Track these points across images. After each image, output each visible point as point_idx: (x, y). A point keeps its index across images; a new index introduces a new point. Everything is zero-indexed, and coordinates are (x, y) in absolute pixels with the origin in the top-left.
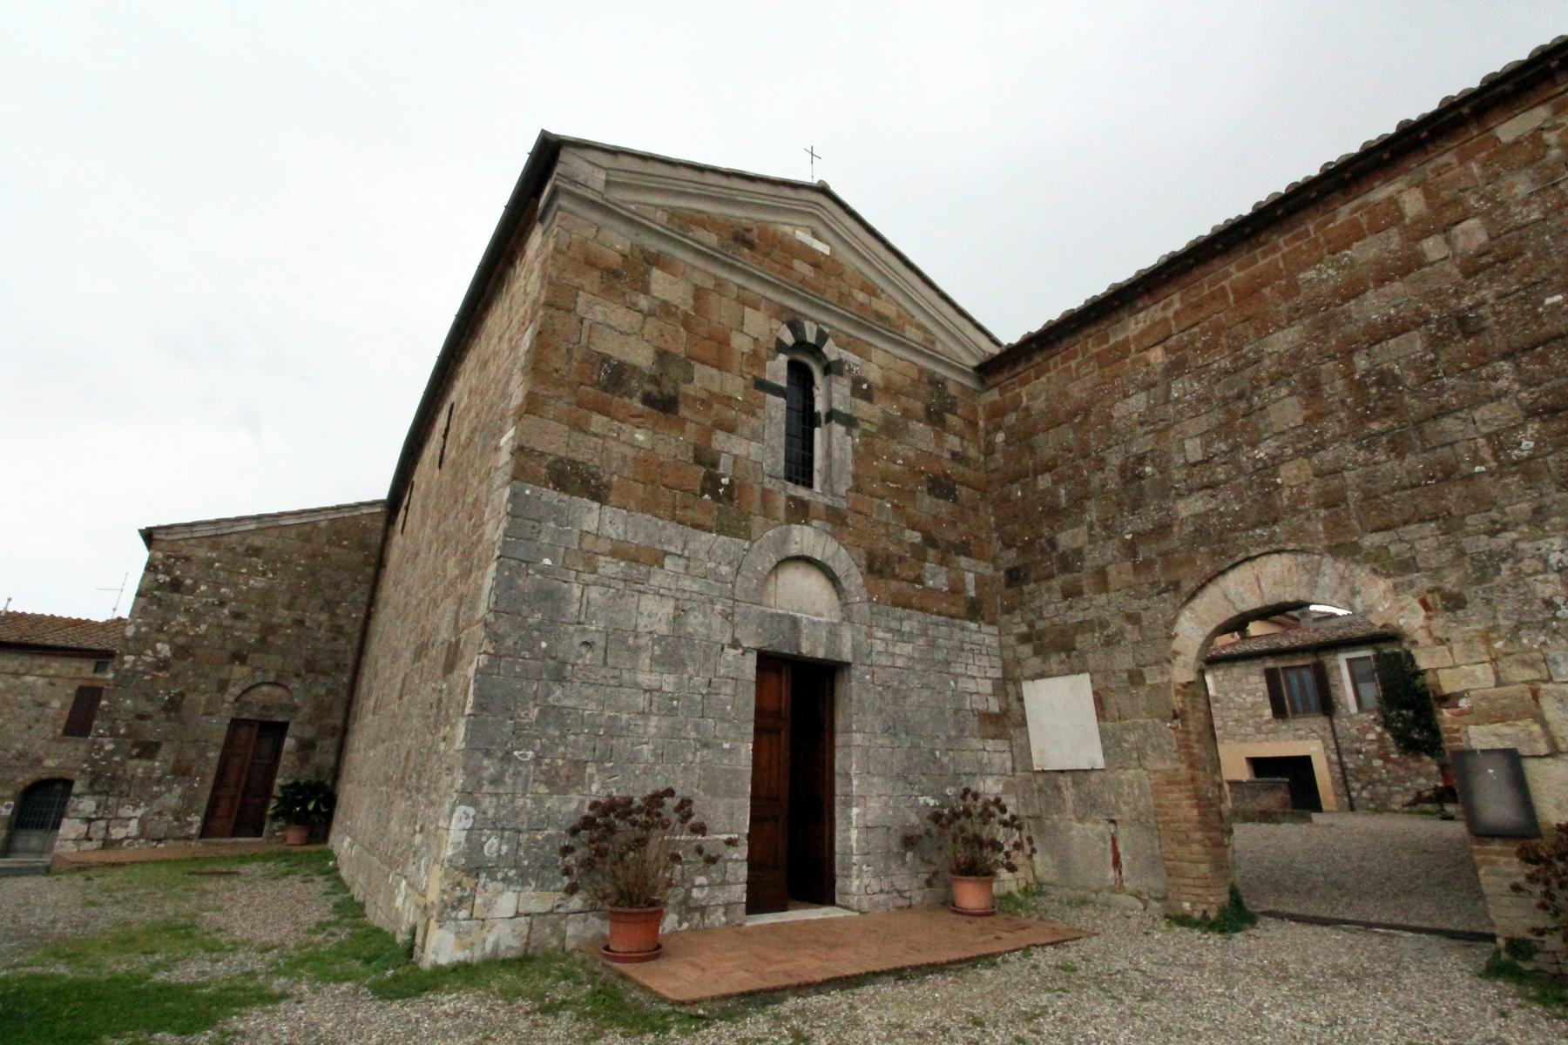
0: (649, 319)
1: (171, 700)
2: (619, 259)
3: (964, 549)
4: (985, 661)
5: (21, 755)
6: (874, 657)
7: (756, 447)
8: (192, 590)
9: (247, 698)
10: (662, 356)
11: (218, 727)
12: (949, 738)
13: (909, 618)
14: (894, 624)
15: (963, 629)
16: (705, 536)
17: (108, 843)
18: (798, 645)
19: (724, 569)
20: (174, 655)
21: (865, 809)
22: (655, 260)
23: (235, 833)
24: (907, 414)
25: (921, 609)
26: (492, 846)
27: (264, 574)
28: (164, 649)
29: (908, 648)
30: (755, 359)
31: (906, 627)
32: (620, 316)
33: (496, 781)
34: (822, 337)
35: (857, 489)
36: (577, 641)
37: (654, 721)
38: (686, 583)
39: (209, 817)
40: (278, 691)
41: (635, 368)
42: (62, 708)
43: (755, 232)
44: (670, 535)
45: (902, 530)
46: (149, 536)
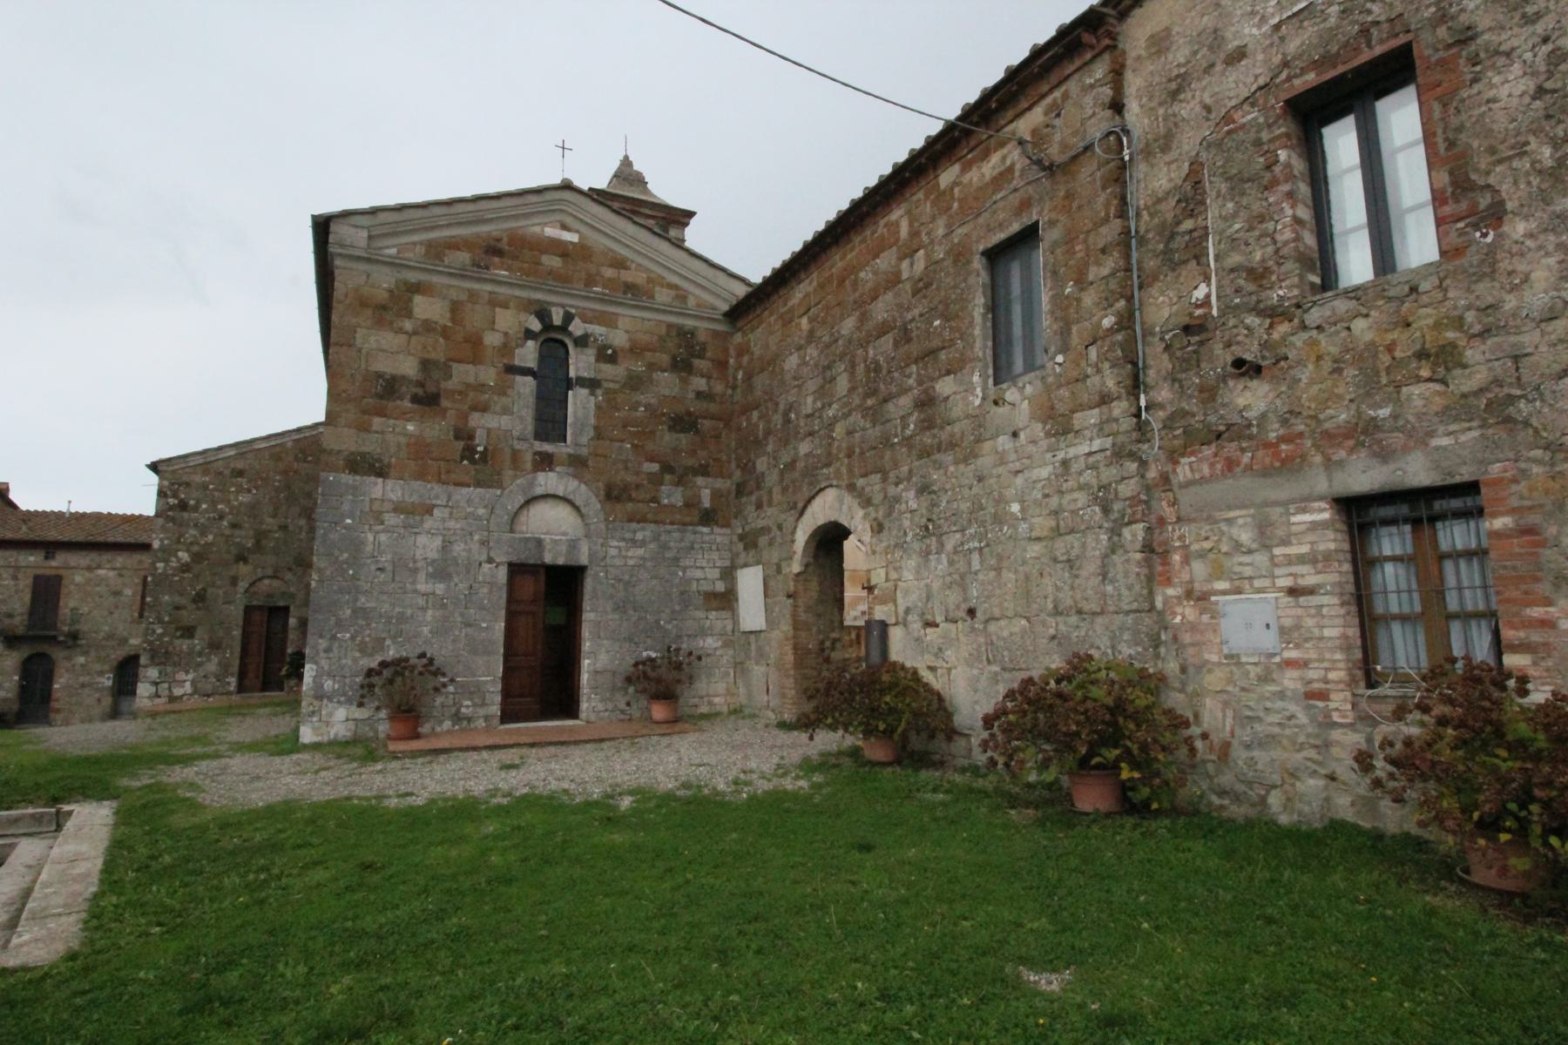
0: (414, 338)
1: (198, 594)
2: (386, 295)
3: (704, 471)
4: (715, 555)
5: (110, 637)
6: (608, 561)
7: (510, 418)
8: (196, 508)
9: (253, 589)
10: (426, 365)
11: (236, 612)
12: (673, 612)
13: (643, 529)
14: (628, 536)
15: (695, 533)
16: (465, 490)
17: (172, 699)
18: (541, 557)
19: (481, 511)
20: (193, 560)
21: (599, 657)
22: (417, 288)
23: (264, 689)
24: (652, 367)
25: (656, 522)
26: (328, 684)
27: (249, 491)
28: (184, 556)
29: (640, 552)
30: (506, 349)
31: (639, 536)
32: (388, 339)
33: (328, 650)
34: (568, 318)
35: (599, 434)
36: (373, 568)
37: (430, 612)
38: (451, 524)
39: (242, 675)
40: (276, 583)
41: (404, 377)
42: (134, 595)
43: (505, 240)
44: (435, 492)
45: (640, 464)
46: (154, 467)
